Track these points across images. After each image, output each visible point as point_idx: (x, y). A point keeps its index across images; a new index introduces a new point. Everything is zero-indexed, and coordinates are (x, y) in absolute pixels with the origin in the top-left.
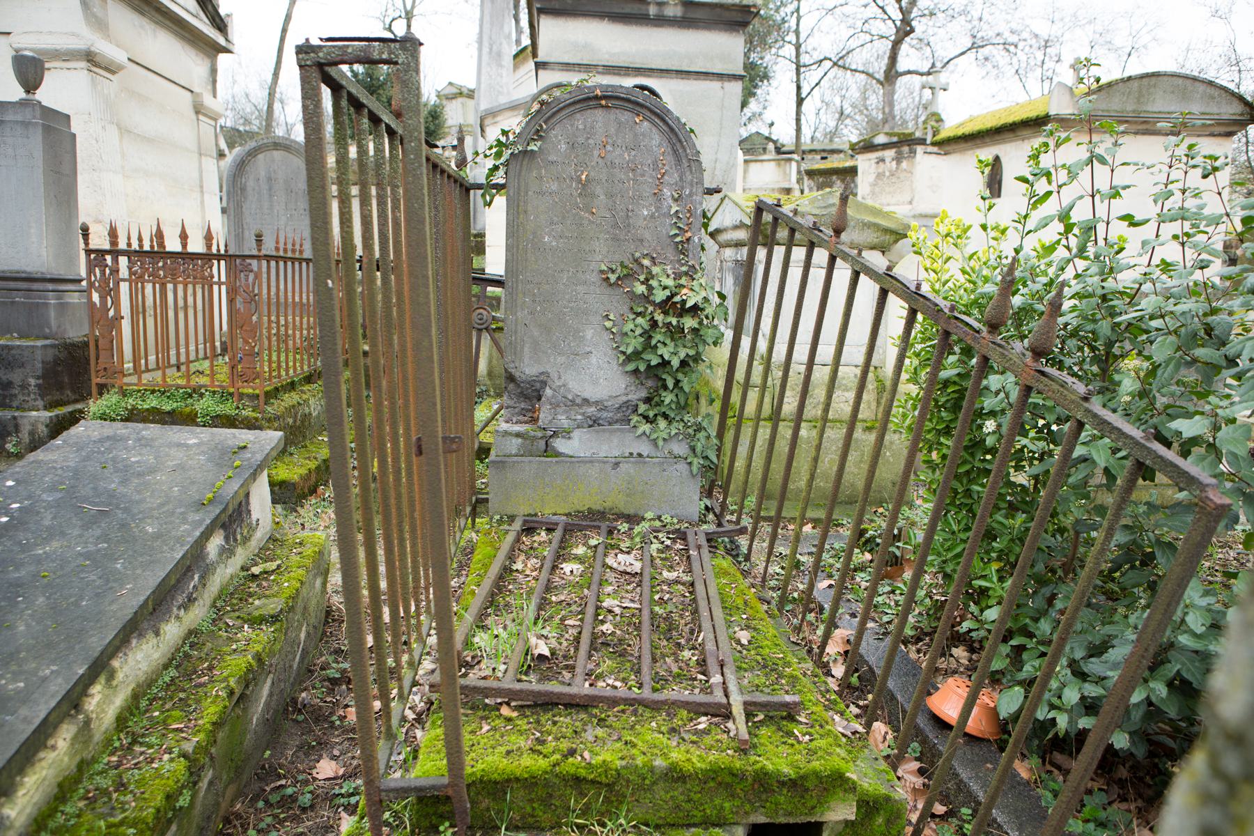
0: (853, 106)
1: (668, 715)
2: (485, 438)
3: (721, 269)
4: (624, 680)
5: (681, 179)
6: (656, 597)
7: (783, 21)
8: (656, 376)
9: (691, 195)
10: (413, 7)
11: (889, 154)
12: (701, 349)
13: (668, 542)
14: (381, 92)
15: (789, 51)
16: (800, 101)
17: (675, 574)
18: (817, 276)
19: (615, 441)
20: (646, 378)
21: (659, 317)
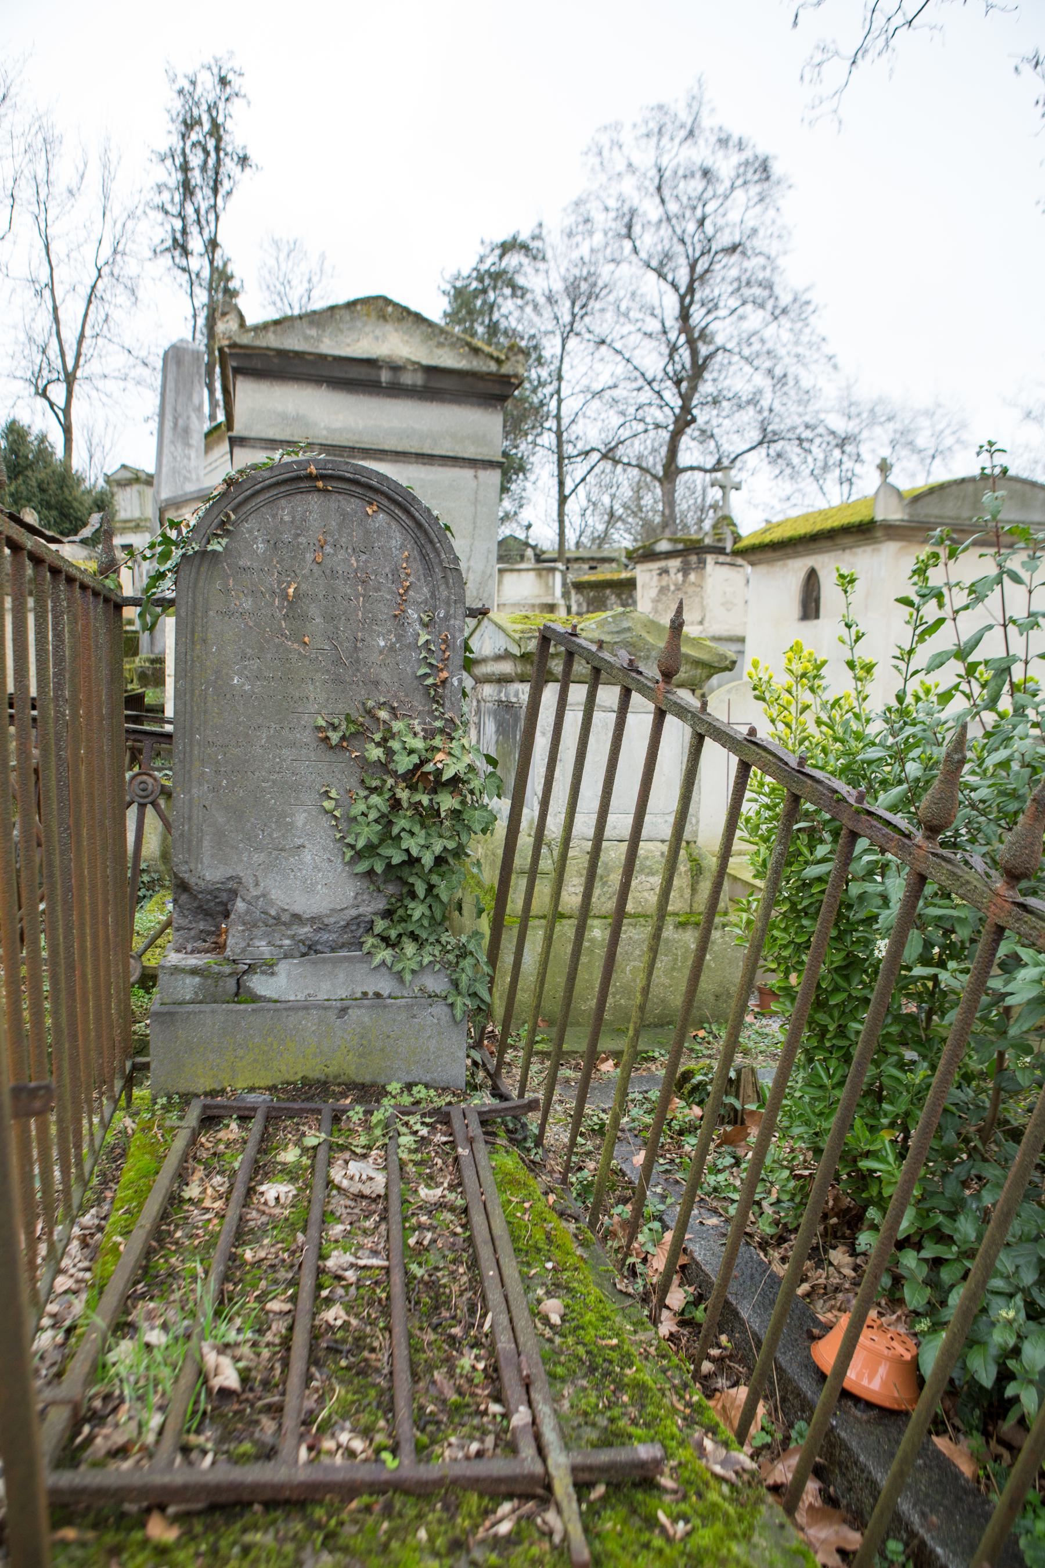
0: (625, 506)
1: (446, 1508)
2: (151, 960)
3: (478, 711)
4: (367, 1433)
5: (433, 596)
6: (412, 1241)
7: (542, 404)
8: (400, 878)
9: (447, 618)
10: (76, 366)
11: (674, 564)
12: (464, 838)
13: (424, 1131)
14: (29, 473)
15: (548, 439)
16: (563, 500)
17: (438, 1192)
18: (604, 721)
19: (342, 976)
20: (385, 882)
21: (403, 795)
